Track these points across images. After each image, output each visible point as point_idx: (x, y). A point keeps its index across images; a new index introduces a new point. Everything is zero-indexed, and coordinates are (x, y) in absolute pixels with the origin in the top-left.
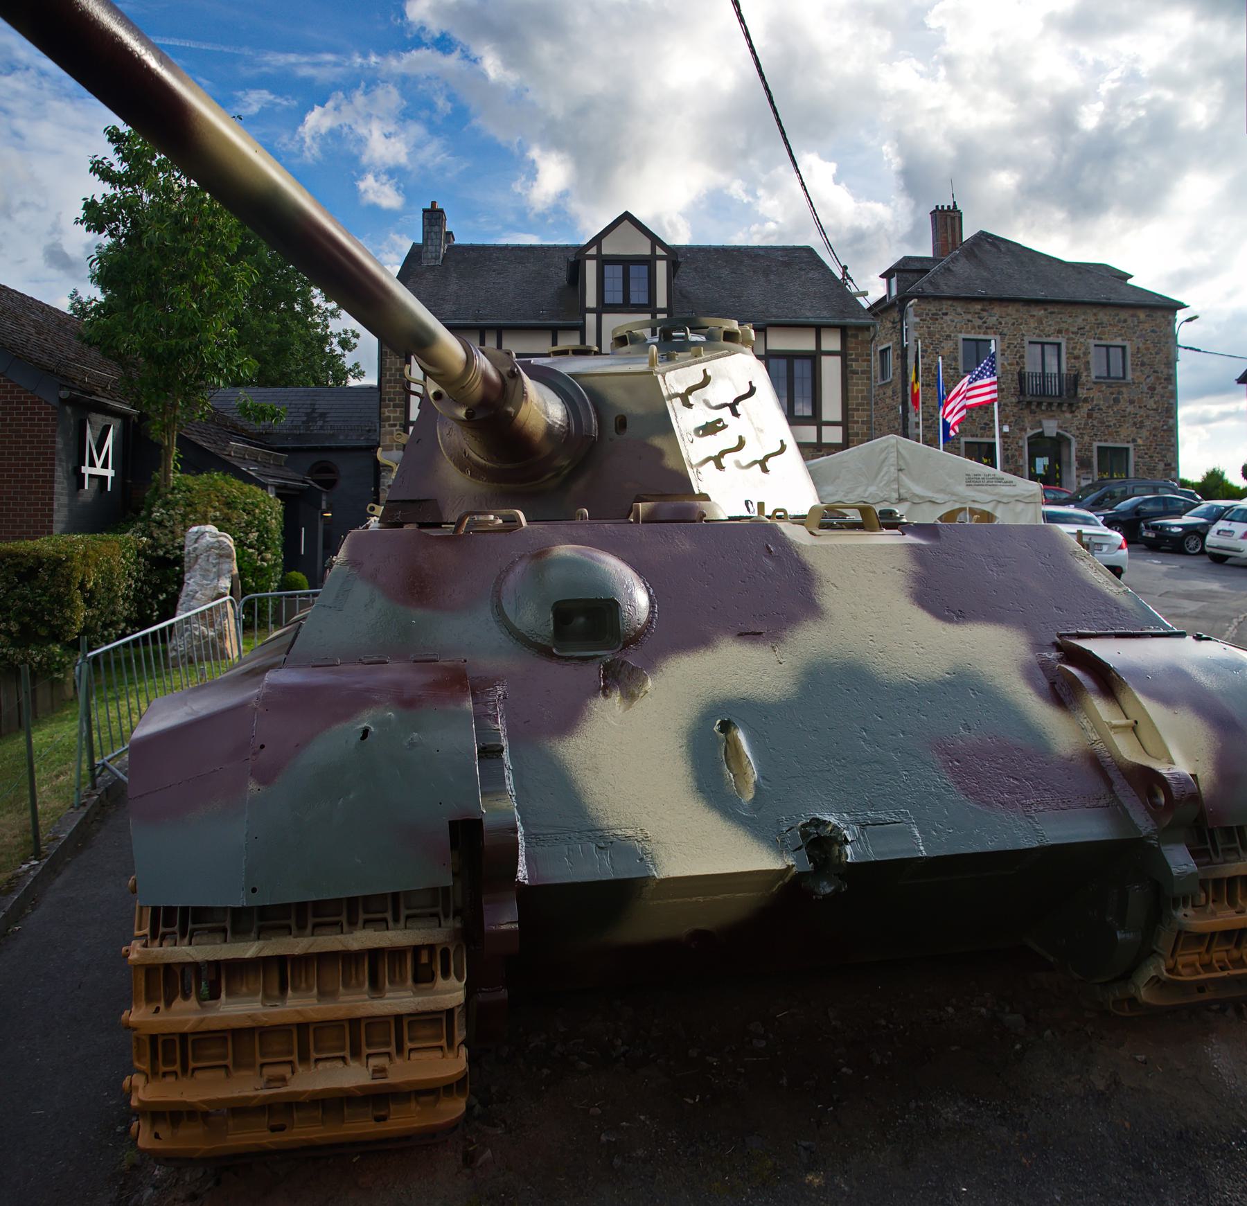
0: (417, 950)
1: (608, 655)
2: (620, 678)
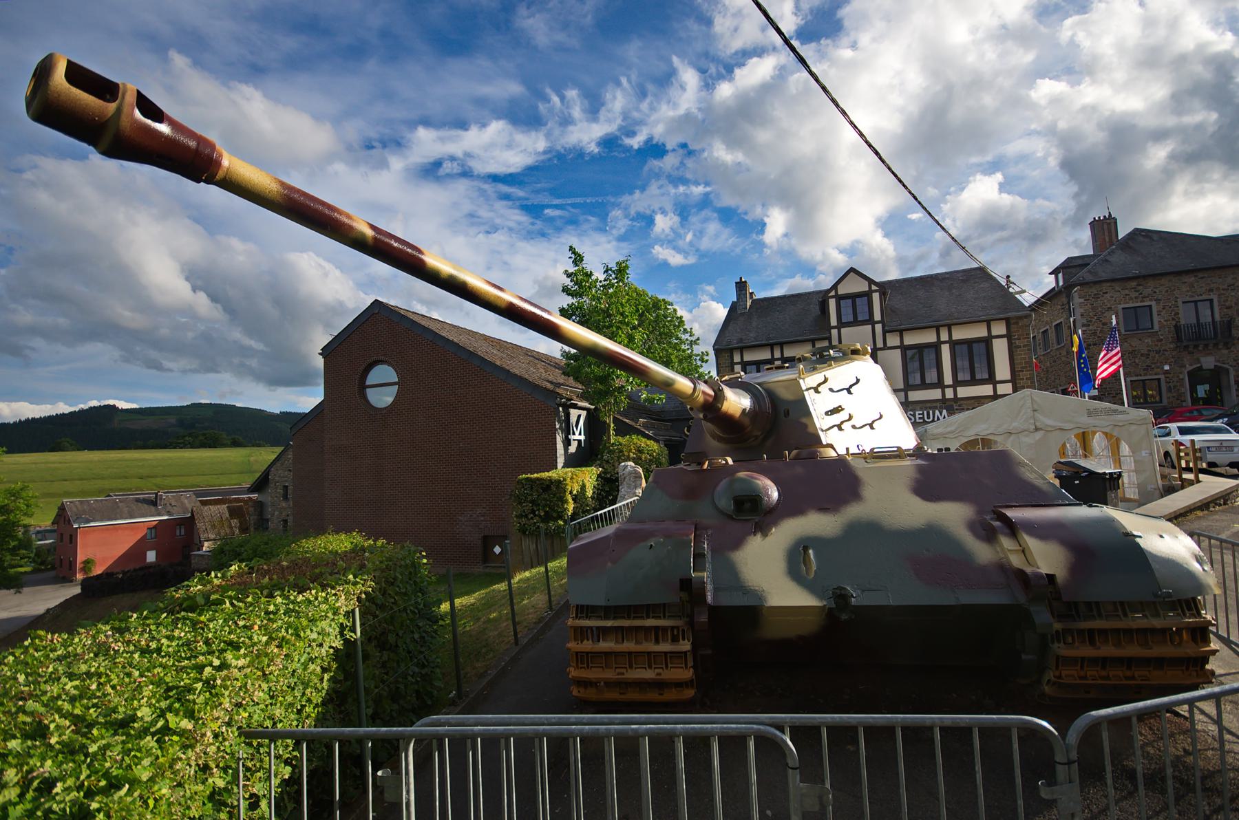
0: (673, 628)
1: (757, 519)
2: (762, 528)
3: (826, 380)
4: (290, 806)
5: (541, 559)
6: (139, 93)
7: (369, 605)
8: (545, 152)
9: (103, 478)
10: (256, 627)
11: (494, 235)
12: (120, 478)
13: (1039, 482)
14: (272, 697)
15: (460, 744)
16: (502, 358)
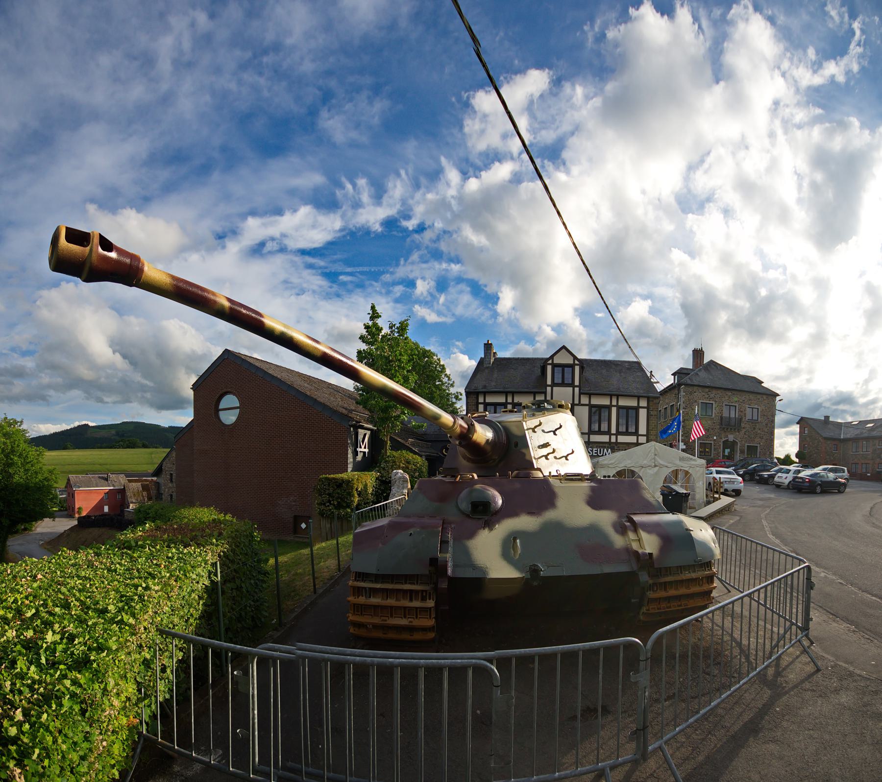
0: (423, 591)
1: (486, 518)
2: (489, 525)
3: (540, 424)
5: (332, 535)
7: (225, 560)
8: (341, 230)
11: (303, 296)
13: (651, 500)
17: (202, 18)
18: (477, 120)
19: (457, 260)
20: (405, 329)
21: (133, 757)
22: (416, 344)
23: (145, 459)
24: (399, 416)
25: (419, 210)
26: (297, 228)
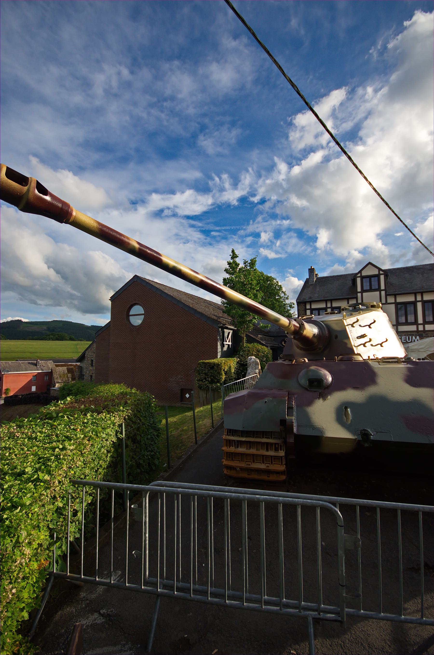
0: (275, 444)
1: (320, 391)
3: (358, 321)
4: (91, 516)
6: (37, 181)
7: (129, 422)
8: (212, 205)
9: (15, 352)
10: (79, 430)
12: (22, 353)
14: (85, 464)
15: (171, 496)
16: (193, 304)
17: (125, 72)
18: (298, 131)
19: (287, 218)
20: (254, 264)
21: (43, 596)
22: (262, 273)
23: (72, 349)
24: (251, 320)
25: (261, 192)
26: (184, 203)
